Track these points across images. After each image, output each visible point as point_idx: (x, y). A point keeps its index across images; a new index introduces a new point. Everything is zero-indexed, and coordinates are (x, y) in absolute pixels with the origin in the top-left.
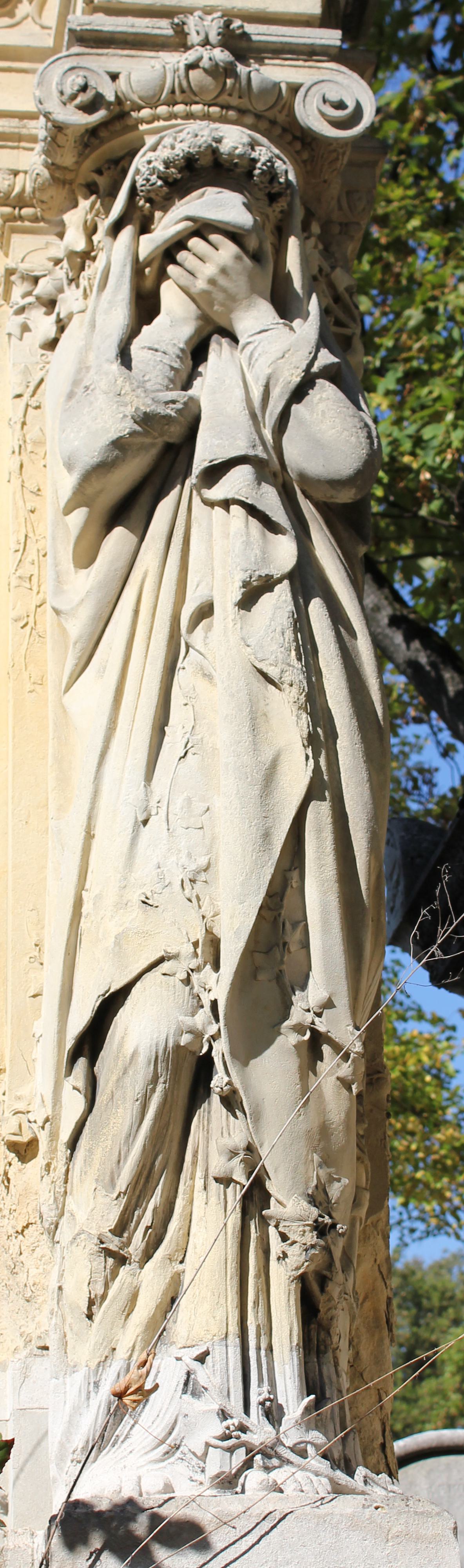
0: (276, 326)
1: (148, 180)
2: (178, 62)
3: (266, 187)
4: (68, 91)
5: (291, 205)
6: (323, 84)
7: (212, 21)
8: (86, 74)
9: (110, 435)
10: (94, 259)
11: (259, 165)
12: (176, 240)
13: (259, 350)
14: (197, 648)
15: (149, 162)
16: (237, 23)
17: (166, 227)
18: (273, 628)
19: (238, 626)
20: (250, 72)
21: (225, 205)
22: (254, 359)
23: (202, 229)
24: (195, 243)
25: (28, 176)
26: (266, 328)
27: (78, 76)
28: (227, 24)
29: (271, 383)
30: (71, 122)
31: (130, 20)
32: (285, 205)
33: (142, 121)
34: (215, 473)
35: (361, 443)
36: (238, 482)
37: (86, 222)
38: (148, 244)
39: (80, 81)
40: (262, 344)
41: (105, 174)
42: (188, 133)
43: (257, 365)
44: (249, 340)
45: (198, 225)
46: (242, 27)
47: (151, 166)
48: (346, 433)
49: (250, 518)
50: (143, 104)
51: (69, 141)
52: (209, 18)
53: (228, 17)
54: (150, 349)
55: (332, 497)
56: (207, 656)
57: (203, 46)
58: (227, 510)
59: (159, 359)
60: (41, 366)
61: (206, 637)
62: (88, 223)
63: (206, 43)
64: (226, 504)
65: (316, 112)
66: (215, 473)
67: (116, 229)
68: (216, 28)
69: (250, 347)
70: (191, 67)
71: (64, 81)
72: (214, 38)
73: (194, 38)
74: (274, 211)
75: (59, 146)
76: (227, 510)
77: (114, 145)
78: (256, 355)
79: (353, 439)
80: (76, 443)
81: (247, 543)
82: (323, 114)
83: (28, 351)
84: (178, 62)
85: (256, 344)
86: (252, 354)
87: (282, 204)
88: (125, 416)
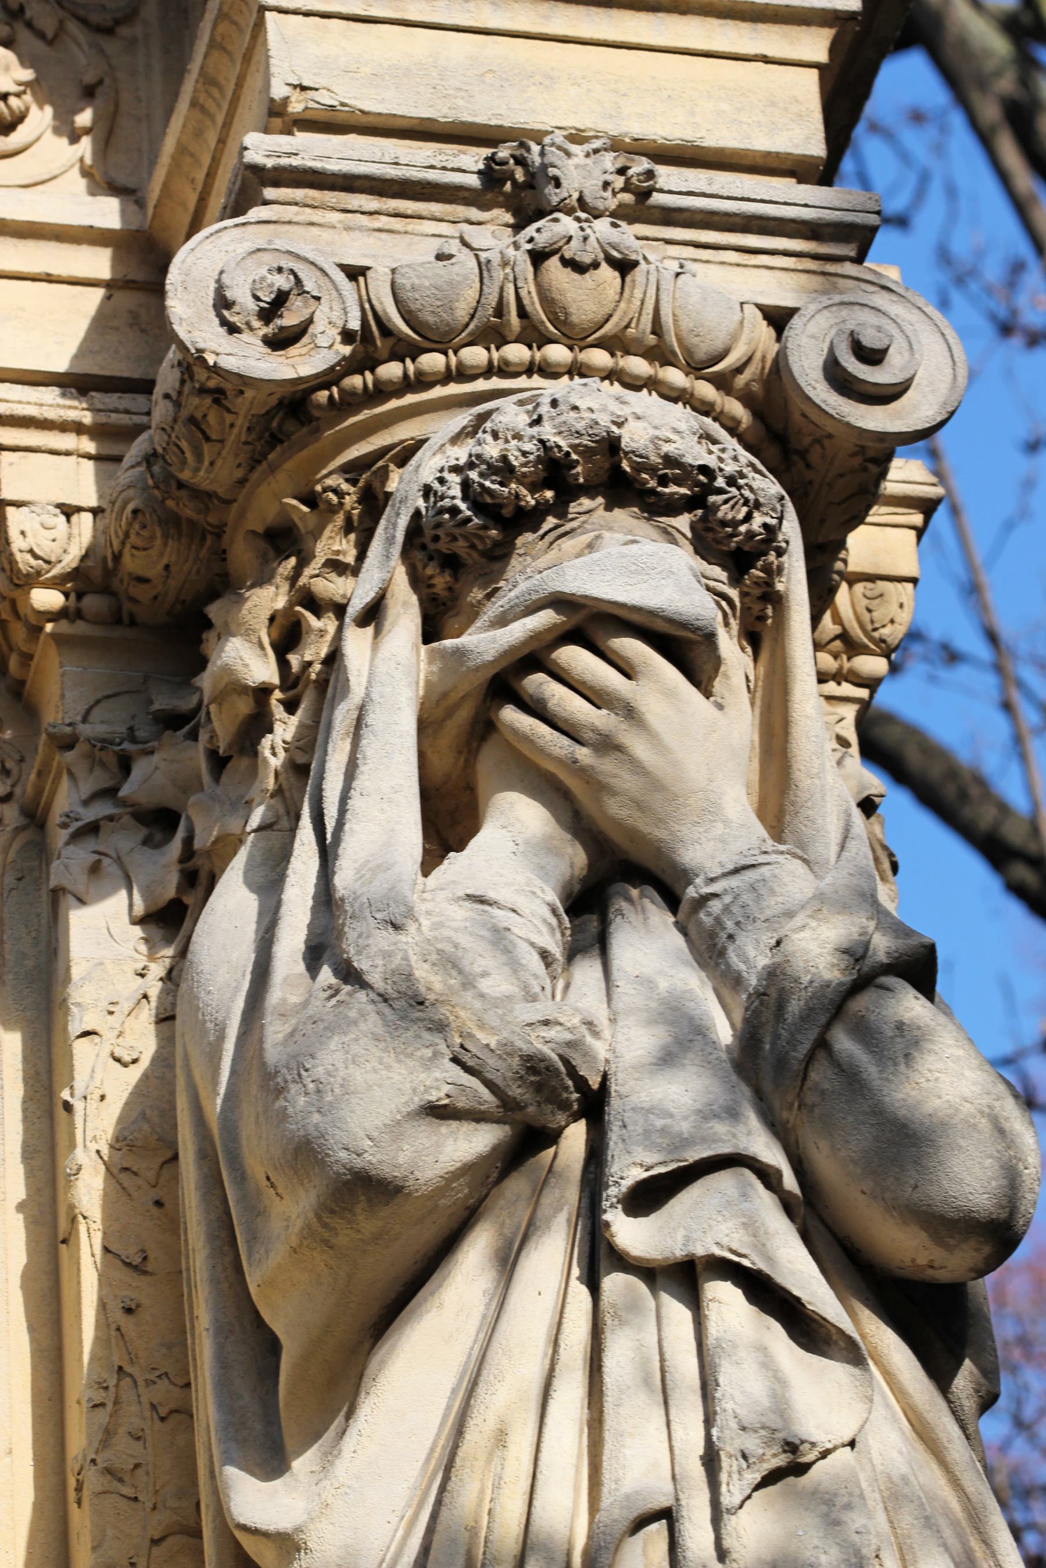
23: (590, 623)
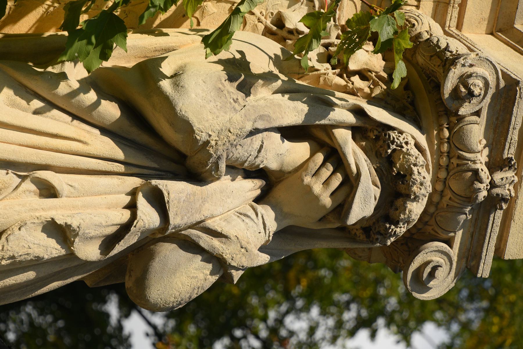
0: (267, 235)
1: (393, 142)
2: (481, 163)
3: (375, 228)
4: (471, 81)
5: (361, 242)
6: (448, 269)
7: (509, 190)
8: (481, 97)
9: (196, 124)
10: (340, 75)
11: (393, 227)
12: (345, 162)
13: (250, 223)
14: (23, 184)
15: (407, 143)
16: (505, 206)
17: (355, 153)
18: (32, 246)
19: (36, 221)
20: (466, 214)
21: (364, 204)
22: (244, 218)
23: (351, 182)
24: (338, 179)
25: (414, 8)
26: (267, 228)
27: (481, 89)
28: (505, 200)
29: (224, 239)
30: (446, 83)
31: (497, 229)
32: (361, 238)
33: (440, 131)
34: (158, 201)
35: (169, 304)
36: (148, 216)
37: (370, 71)
38: (343, 136)
39: (477, 91)
40: (255, 225)
41: (404, 92)
42: (424, 178)
43: (239, 221)
44: (260, 215)
45: (353, 182)
46: (501, 208)
47: (404, 145)
48: (178, 294)
49: (119, 226)
50: (452, 133)
51: (434, 65)
52: (511, 188)
53: (511, 201)
54: (261, 146)
55: (130, 276)
56: (15, 193)
57: (490, 183)
58: (126, 207)
59: (252, 153)
60: (264, 14)
61: (30, 192)
62: (370, 73)
63: (493, 185)
64: (132, 207)
65: (429, 259)
66: (158, 201)
67: (358, 112)
68: (503, 193)
69: (253, 216)
70: (476, 172)
71: (479, 78)
72: (496, 191)
73: (498, 176)
74: (357, 230)
75: (431, 56)
76: (126, 207)
77: (425, 105)
78: (247, 220)
79: (172, 299)
80: (193, 96)
81: (100, 226)
82: (427, 263)
83: (277, 3)
84: (481, 163)
85: (256, 220)
86: (248, 216)
87: (363, 237)
88: (210, 136)
